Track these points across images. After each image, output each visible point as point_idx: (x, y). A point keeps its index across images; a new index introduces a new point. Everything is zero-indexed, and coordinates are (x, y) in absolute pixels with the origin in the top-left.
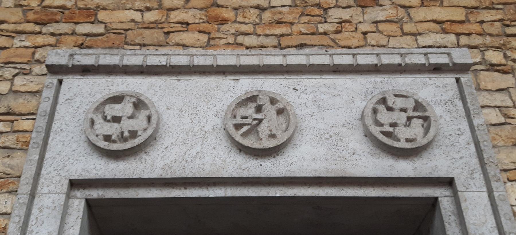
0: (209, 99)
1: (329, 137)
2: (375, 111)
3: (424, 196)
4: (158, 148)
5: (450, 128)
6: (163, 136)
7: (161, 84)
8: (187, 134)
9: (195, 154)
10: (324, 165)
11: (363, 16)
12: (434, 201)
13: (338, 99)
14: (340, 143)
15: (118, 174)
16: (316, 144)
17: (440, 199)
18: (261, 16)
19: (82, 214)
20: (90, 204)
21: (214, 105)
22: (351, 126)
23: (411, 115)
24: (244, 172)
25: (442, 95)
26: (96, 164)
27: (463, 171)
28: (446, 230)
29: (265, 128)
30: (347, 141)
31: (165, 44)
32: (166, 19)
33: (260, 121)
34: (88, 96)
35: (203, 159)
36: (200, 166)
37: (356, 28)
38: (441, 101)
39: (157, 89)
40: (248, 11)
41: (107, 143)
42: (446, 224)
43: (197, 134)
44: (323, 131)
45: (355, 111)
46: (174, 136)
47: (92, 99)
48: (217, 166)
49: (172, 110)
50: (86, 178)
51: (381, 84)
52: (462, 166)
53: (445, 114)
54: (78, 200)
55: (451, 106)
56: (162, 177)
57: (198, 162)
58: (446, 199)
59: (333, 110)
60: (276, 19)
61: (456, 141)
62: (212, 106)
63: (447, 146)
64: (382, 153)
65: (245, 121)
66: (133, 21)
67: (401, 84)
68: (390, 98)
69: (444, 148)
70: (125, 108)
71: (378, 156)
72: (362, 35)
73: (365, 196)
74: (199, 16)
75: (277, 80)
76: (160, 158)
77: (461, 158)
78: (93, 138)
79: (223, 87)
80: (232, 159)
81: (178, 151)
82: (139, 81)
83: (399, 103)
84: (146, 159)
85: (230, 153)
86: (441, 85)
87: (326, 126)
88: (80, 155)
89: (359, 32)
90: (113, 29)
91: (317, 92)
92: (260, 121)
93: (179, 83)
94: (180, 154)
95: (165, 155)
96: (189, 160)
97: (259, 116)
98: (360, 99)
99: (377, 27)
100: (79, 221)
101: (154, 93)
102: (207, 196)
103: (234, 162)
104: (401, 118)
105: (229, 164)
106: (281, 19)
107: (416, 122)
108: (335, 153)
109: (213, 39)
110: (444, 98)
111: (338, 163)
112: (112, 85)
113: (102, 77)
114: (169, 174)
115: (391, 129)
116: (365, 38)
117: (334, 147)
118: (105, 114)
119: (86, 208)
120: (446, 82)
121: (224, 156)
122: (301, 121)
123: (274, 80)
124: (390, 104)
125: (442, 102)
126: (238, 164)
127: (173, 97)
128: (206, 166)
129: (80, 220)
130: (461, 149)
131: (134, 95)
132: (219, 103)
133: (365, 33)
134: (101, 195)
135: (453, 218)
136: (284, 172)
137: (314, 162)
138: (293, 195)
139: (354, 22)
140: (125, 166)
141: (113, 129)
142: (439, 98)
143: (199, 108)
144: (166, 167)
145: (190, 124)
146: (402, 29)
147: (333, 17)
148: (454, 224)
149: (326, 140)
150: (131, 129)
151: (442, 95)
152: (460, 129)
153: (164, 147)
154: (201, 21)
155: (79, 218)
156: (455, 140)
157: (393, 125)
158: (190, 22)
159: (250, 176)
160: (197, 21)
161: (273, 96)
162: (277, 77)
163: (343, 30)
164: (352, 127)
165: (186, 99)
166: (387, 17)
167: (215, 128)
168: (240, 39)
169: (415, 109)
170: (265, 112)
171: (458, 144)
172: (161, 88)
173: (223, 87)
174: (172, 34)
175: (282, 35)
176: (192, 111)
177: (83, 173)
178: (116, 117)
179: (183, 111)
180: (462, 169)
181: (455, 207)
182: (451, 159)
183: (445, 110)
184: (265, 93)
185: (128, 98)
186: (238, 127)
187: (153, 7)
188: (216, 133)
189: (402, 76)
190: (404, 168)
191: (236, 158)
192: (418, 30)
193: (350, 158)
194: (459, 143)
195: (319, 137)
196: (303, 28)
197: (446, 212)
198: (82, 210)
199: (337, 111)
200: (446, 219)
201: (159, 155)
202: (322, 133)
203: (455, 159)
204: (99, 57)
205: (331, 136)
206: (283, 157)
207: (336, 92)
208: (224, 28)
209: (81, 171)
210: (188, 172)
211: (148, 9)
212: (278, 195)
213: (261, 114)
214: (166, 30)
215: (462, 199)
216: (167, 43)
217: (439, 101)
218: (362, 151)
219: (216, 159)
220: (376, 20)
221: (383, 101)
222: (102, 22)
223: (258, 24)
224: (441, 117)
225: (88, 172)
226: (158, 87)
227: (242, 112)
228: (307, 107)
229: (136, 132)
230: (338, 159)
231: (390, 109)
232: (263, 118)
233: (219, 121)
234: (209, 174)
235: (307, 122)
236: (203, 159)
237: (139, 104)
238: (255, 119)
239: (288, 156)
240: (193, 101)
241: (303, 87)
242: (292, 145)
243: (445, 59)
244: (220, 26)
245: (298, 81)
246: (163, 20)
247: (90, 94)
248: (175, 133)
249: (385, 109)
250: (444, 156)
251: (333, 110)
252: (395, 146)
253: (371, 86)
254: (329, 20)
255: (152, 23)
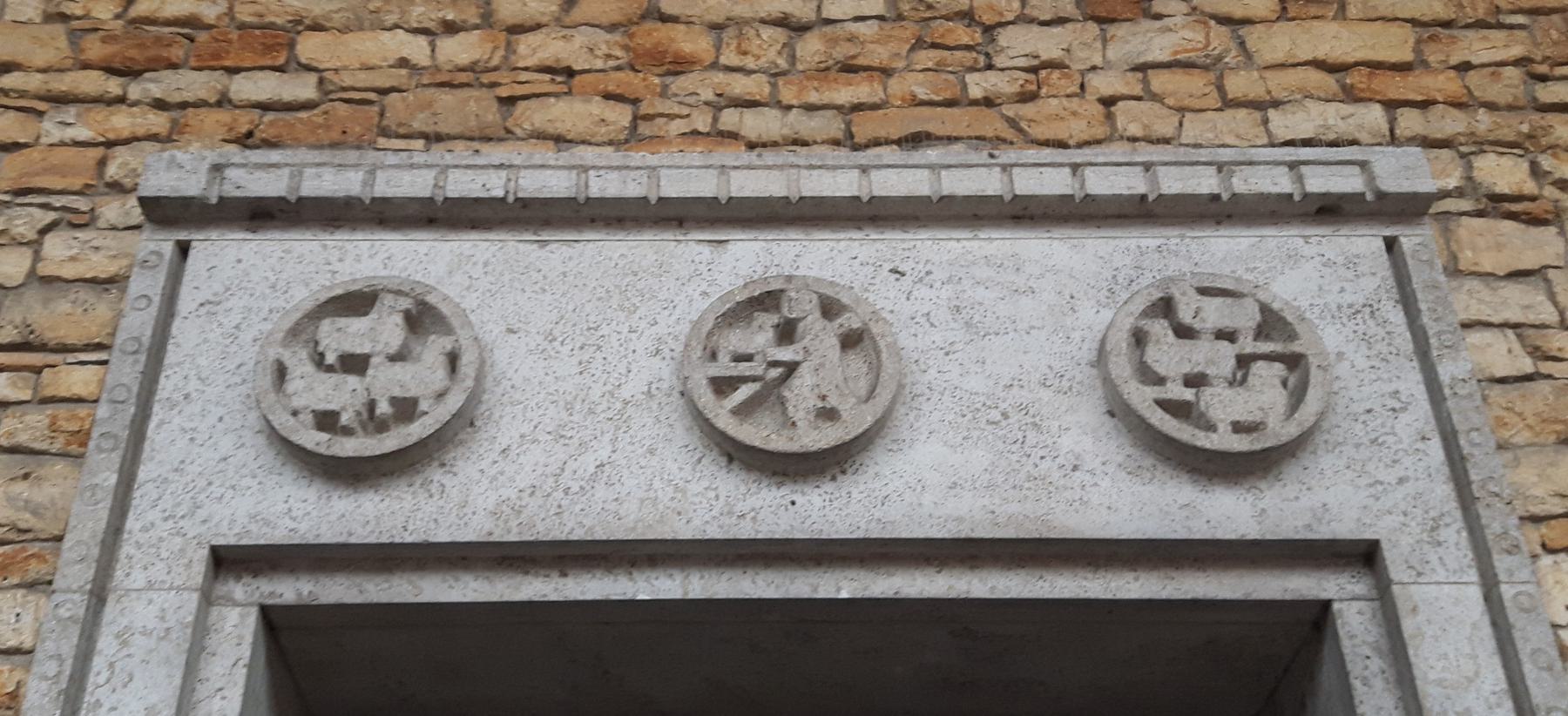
0: (636, 300)
1: (999, 417)
2: (1139, 339)
3: (1288, 597)
4: (482, 451)
5: (1366, 390)
6: (497, 415)
7: (488, 255)
8: (569, 408)
9: (592, 469)
10: (986, 501)
11: (1104, 47)
12: (1321, 612)
13: (1026, 302)
14: (1032, 437)
15: (360, 530)
16: (959, 439)
17: (1336, 606)
18: (794, 50)
19: (248, 654)
20: (273, 620)
21: (650, 319)
22: (1065, 384)
23: (1248, 350)
24: (743, 523)
25: (1342, 290)
26: (291, 500)
27: (1407, 520)
28: (1357, 701)
29: (806, 391)
30: (1054, 429)
31: (502, 133)
32: (506, 58)
33: (791, 368)
34: (268, 291)
35: (618, 486)
36: (607, 506)
37: (1082, 86)
38: (1339, 307)
39: (477, 272)
40: (752, 32)
41: (324, 436)
42: (1357, 684)
43: (599, 409)
44: (982, 399)
45: (1078, 339)
46: (529, 414)
47: (281, 303)
48: (661, 507)
49: (522, 334)
50: (262, 542)
51: (1157, 255)
52: (1403, 506)
53: (1352, 347)
54: (238, 609)
55: (1371, 323)
56: (491, 539)
57: (601, 492)
58: (1356, 605)
59: (1012, 334)
60: (840, 57)
61: (1387, 430)
62: (643, 324)
63: (1357, 446)
64: (1160, 468)
65: (744, 369)
66: (403, 63)
67: (1220, 255)
68: (1185, 299)
69: (1349, 450)
70: (381, 330)
71: (1149, 475)
72: (1100, 107)
73: (1109, 596)
74: (604, 49)
75: (843, 244)
76: (485, 482)
77: (1401, 481)
78: (283, 421)
79: (677, 267)
80: (706, 483)
81: (542, 460)
82: (423, 248)
83: (1214, 313)
84: (443, 485)
85: (699, 467)
86: (1340, 260)
87: (991, 383)
88: (245, 471)
89: (1091, 97)
90: (344, 89)
91: (964, 282)
92: (791, 368)
93: (543, 253)
94: (548, 470)
95: (502, 473)
96: (575, 488)
97: (786, 354)
98: (1093, 302)
99: (1146, 82)
100: (241, 673)
101: (467, 284)
102: (629, 596)
103: (712, 494)
104: (1218, 359)
105: (697, 500)
106: (854, 57)
107: (1264, 373)
108: (1017, 466)
109: (649, 118)
110: (1348, 298)
111: (1026, 497)
112: (341, 260)
113: (308, 235)
114: (515, 530)
115: (1188, 394)
116: (1110, 117)
117: (1014, 448)
118: (321, 349)
119: (261, 633)
120: (1355, 251)
121: (682, 474)
122: (914, 367)
123: (832, 244)
124: (1185, 316)
125: (1345, 309)
126: (722, 499)
127: (527, 295)
128: (625, 505)
129: (244, 671)
130: (1401, 453)
131: (406, 289)
132: (666, 313)
133: (1108, 102)
134: (306, 593)
135: (1376, 664)
136: (863, 525)
137: (953, 492)
138: (890, 594)
139: (1076, 66)
140: (381, 506)
141: (342, 394)
142: (1333, 299)
143: (605, 330)
144: (504, 508)
145: (578, 379)
146: (1220, 88)
147: (1011, 53)
148: (1378, 684)
149: (990, 427)
150: (397, 392)
151: (1342, 290)
152: (1397, 392)
153: (498, 448)
154: (612, 63)
155: (241, 663)
156: (1383, 425)
157: (1196, 381)
158: (576, 67)
159: (760, 536)
160: (599, 64)
161: (829, 292)
162: (842, 236)
163: (1044, 91)
164: (1070, 388)
165: (564, 300)
166: (1176, 53)
167: (654, 391)
168: (729, 118)
169: (1261, 333)
170: (805, 342)
171: (1390, 439)
172: (490, 268)
173: (677, 267)
174: (522, 104)
175: (858, 108)
176: (582, 339)
177: (253, 527)
178: (352, 356)
179: (555, 339)
180: (1405, 514)
181: (1383, 631)
182: (1371, 485)
183: (1352, 336)
184: (806, 284)
185: (388, 300)
186: (722, 386)
187: (464, 21)
188: (655, 407)
189: (1222, 232)
190: (1229, 512)
191: (718, 483)
192: (1269, 92)
193: (1062, 482)
194: (1395, 434)
195: (969, 416)
196: (921, 85)
197: (1354, 646)
198: (249, 639)
199: (1025, 337)
200: (1354, 667)
201: (482, 471)
202: (979, 406)
203: (1381, 483)
204: (301, 173)
205: (1005, 415)
206: (861, 478)
207: (1020, 281)
208: (680, 84)
209: (246, 521)
210: (570, 525)
211: (451, 28)
212: (844, 595)
213: (792, 348)
214: (504, 92)
215: (1403, 607)
216: (508, 131)
217: (1334, 307)
218: (1100, 459)
219: (657, 484)
220: (1142, 60)
221: (1165, 307)
222: (309, 68)
223: (783, 73)
224: (1340, 355)
225: (267, 523)
226: (480, 266)
227: (736, 340)
228: (932, 325)
229: (414, 402)
230: (1027, 485)
231: (1184, 332)
232: (798, 358)
233: (664, 370)
234: (634, 529)
235: (933, 372)
236: (618, 486)
237: (422, 318)
238: (775, 364)
239: (876, 474)
240: (588, 308)
241: (920, 266)
242: (887, 440)
243: (1351, 180)
244: (669, 79)
245: (905, 246)
246: (495, 62)
247: (273, 287)
248: (533, 404)
249: (1170, 332)
250: (1350, 474)
251: (1012, 334)
252: (1199, 444)
253: (1128, 261)
254: (999, 61)
255: (462, 70)
